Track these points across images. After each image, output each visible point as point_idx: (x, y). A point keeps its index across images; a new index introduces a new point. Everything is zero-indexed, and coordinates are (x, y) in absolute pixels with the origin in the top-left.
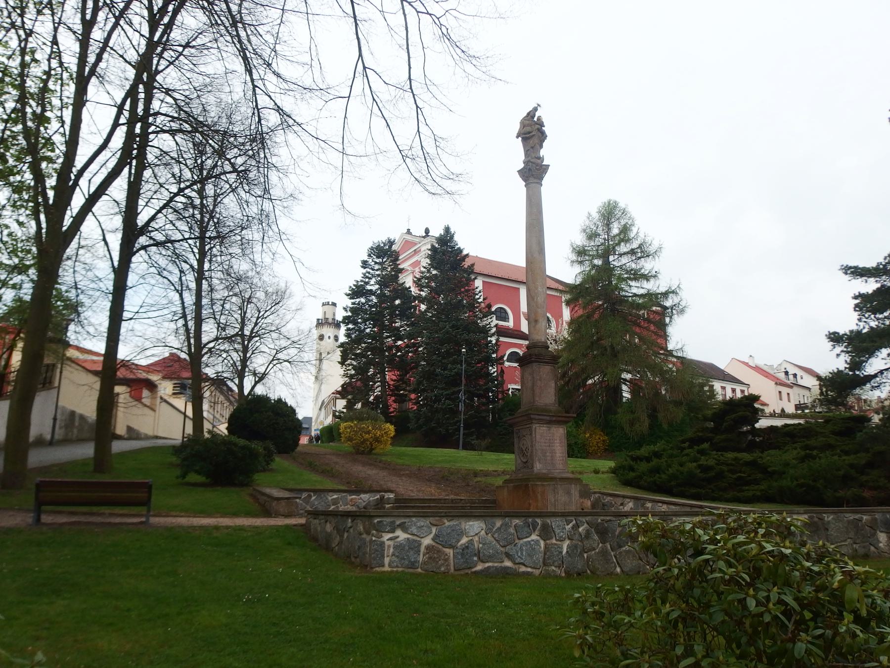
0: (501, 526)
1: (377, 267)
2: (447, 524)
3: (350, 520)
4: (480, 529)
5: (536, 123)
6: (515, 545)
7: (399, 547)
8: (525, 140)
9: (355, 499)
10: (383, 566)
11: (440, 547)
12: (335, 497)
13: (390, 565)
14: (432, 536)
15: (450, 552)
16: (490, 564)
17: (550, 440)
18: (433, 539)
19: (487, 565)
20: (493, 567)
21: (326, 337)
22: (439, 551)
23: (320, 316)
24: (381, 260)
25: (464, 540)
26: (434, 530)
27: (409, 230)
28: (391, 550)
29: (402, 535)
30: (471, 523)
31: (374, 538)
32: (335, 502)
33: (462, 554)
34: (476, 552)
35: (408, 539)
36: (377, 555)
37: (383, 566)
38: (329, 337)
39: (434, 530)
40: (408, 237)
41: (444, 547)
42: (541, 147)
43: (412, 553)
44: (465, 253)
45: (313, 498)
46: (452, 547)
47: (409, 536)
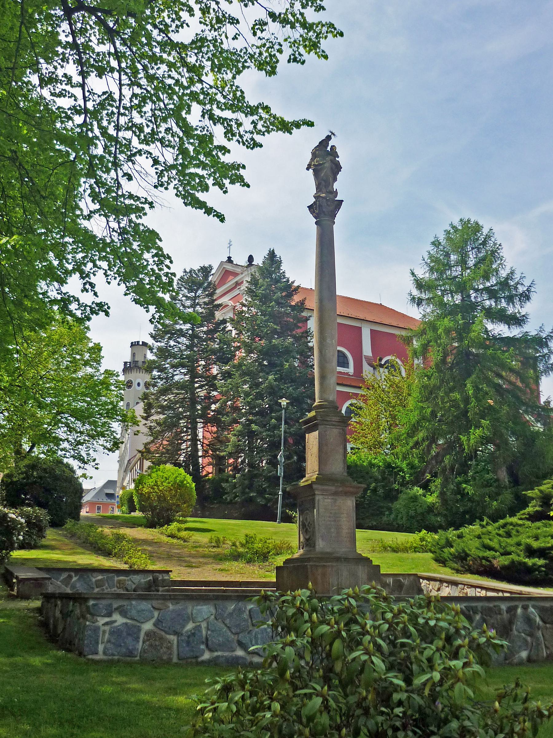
0: (234, 610)
1: (188, 303)
2: (171, 607)
3: (71, 603)
4: (209, 614)
5: (328, 153)
6: (249, 633)
7: (116, 633)
8: (316, 174)
9: (125, 580)
10: (97, 653)
11: (163, 633)
12: (100, 577)
13: (105, 653)
14: (154, 620)
15: (173, 638)
16: (219, 653)
17: (335, 513)
18: (155, 625)
19: (216, 654)
20: (222, 657)
21: (135, 384)
22: (161, 638)
23: (128, 359)
24: (193, 294)
25: (190, 626)
26: (156, 614)
27: (229, 258)
28: (107, 635)
29: (119, 620)
30: (199, 607)
31: (88, 623)
32: (99, 584)
33: (188, 643)
34: (204, 640)
35: (126, 624)
36: (91, 641)
37: (97, 653)
38: (139, 384)
39: (156, 614)
40: (229, 267)
41: (166, 633)
42: (335, 180)
43: (130, 639)
44: (296, 284)
45: (74, 579)
46: (176, 633)
47: (128, 621)
